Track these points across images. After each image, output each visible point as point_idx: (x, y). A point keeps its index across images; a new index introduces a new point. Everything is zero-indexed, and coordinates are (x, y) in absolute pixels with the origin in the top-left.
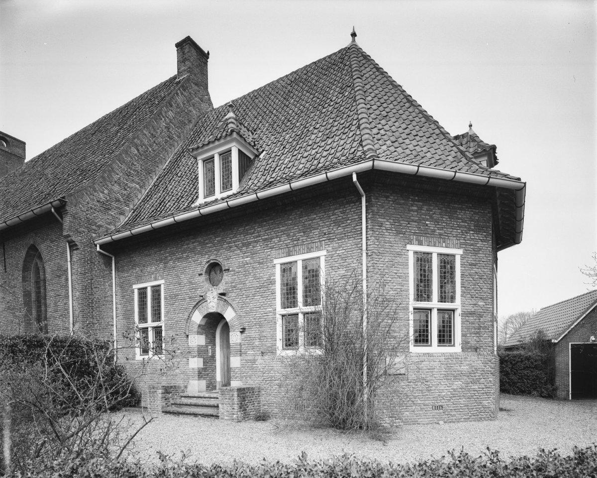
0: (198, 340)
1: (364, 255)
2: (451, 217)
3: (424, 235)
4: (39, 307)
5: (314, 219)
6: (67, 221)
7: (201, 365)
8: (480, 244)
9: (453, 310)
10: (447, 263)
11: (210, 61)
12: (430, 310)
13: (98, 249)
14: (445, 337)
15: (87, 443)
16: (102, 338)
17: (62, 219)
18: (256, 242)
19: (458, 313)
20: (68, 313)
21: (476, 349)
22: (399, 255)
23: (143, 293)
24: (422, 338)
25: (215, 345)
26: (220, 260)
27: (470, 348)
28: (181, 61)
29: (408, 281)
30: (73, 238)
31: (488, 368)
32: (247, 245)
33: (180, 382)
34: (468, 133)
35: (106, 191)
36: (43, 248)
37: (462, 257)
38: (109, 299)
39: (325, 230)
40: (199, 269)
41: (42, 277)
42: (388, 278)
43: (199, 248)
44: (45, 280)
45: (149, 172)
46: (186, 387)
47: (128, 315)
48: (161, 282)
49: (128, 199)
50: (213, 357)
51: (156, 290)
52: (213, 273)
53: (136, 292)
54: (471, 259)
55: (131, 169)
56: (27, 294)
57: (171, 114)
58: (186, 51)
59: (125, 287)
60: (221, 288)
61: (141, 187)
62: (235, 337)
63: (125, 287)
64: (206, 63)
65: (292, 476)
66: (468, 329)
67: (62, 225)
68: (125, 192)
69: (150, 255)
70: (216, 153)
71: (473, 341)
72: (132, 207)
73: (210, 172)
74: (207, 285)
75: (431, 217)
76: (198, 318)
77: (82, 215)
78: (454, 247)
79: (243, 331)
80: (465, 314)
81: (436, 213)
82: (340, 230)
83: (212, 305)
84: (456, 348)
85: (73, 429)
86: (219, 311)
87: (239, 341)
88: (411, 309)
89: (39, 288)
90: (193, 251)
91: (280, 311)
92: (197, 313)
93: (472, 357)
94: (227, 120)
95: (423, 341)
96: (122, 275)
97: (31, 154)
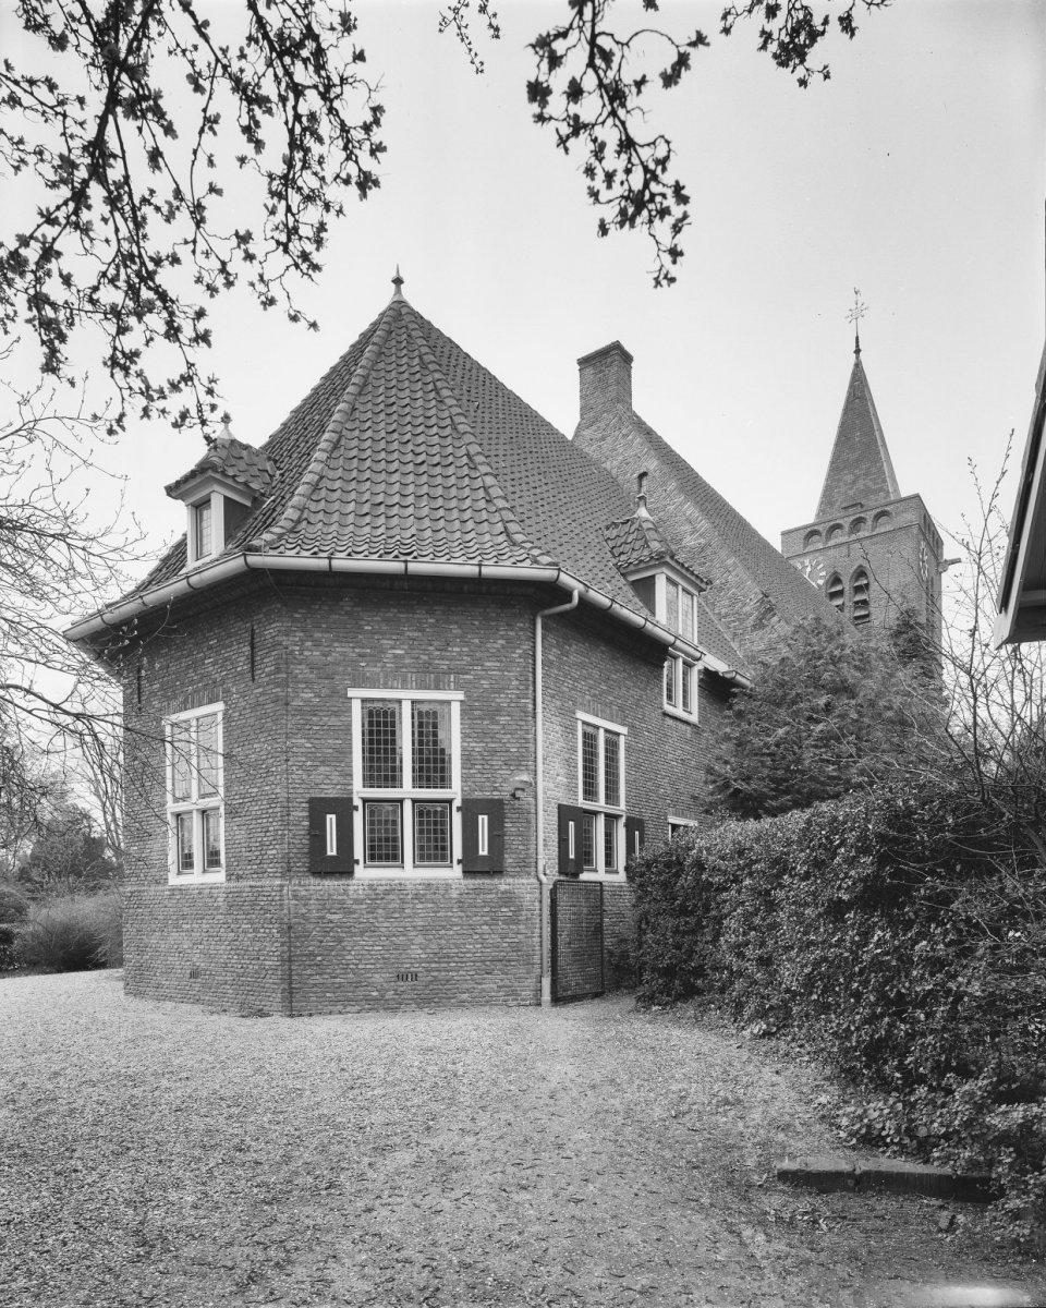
9: (450, 802)
12: (401, 801)
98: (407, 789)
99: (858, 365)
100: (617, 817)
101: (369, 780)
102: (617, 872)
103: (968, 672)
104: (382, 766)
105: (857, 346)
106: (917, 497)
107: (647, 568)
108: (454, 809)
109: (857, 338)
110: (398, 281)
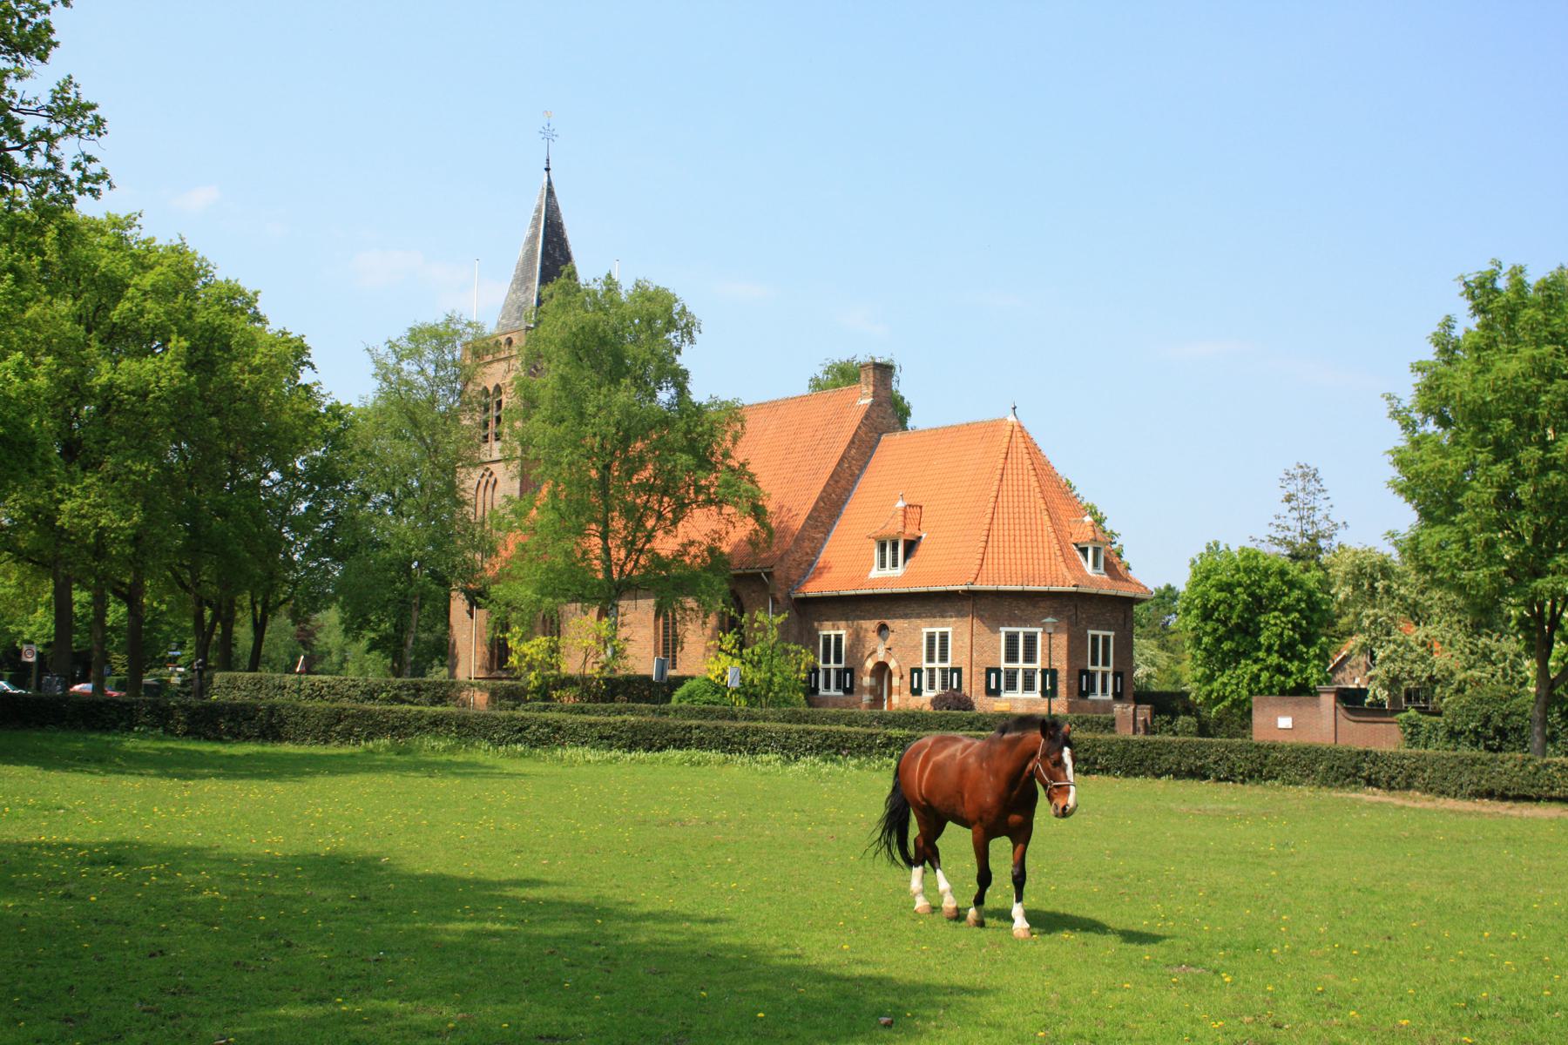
2: (1034, 606)
15: (1540, 959)
23: (1095, 638)
43: (873, 611)
48: (949, 630)
51: (944, 637)
60: (889, 643)
65: (1100, 1042)
83: (881, 656)
86: (886, 661)
92: (870, 660)
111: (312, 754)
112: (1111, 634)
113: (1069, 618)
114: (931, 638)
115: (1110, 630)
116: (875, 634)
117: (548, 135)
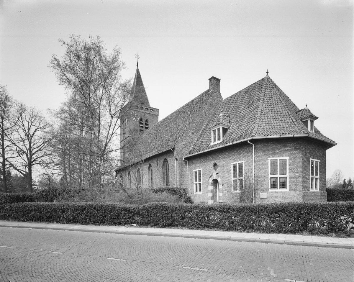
0: (211, 188)
1: (254, 162)
2: (285, 147)
3: (274, 153)
4: (167, 177)
5: (241, 151)
6: (175, 152)
7: (212, 195)
8: (297, 154)
9: (286, 177)
10: (283, 163)
11: (221, 82)
12: (277, 177)
13: (183, 159)
14: (283, 185)
16: (184, 187)
17: (174, 151)
18: (227, 157)
19: (288, 178)
20: (175, 179)
21: (295, 190)
22: (265, 161)
23: (312, 162)
24: (274, 186)
25: (216, 189)
26: (217, 163)
27: (293, 190)
28: (211, 85)
29: (268, 169)
30: (177, 157)
31: (299, 196)
32: (224, 158)
33: (206, 201)
34: (304, 109)
35: (186, 141)
36: (168, 159)
37: (289, 160)
38: (186, 174)
39: (244, 154)
40: (211, 165)
41: (168, 168)
42: (261, 169)
44: (169, 169)
45: (199, 130)
46: (207, 202)
47: (192, 180)
48: (243, 161)
49: (192, 141)
50: (216, 193)
51: (200, 172)
52: (215, 166)
53: (194, 172)
54: (293, 160)
55: (193, 131)
56: (164, 173)
57: (206, 107)
58: (212, 81)
59: (191, 170)
60: (217, 171)
61: (196, 136)
62: (221, 187)
63: (191, 170)
64: (219, 83)
66: (292, 183)
67: (174, 153)
68: (192, 139)
69: (198, 161)
70: (216, 129)
71: (294, 187)
72: (193, 143)
73: (215, 134)
74: (214, 170)
75: (277, 148)
76: (211, 181)
77: (179, 150)
78: (286, 156)
79: (223, 185)
80: (290, 178)
81: (279, 146)
82: (248, 154)
83: (215, 177)
84: (287, 190)
85: (183, 194)
86: (216, 179)
87: (222, 188)
88: (269, 178)
89: (167, 171)
90: (210, 159)
91: (233, 179)
93: (293, 192)
94: (220, 117)
95: (284, 188)
96: (190, 166)
97: (161, 118)
98: (278, 175)
99: (138, 69)
100: (317, 178)
101: (271, 174)
102: (317, 189)
103: (69, 151)
104: (274, 172)
105: (137, 65)
106: (220, 80)
107: (306, 119)
108: (287, 179)
109: (137, 63)
110: (267, 72)
111: (90, 206)
112: (319, 161)
113: (302, 152)
114: (235, 167)
115: (318, 159)
116: (212, 168)
117: (137, 57)
